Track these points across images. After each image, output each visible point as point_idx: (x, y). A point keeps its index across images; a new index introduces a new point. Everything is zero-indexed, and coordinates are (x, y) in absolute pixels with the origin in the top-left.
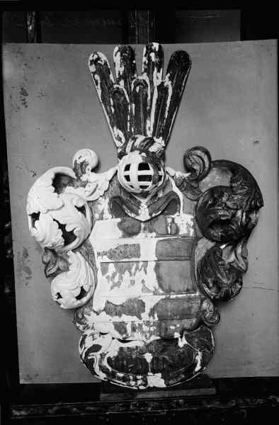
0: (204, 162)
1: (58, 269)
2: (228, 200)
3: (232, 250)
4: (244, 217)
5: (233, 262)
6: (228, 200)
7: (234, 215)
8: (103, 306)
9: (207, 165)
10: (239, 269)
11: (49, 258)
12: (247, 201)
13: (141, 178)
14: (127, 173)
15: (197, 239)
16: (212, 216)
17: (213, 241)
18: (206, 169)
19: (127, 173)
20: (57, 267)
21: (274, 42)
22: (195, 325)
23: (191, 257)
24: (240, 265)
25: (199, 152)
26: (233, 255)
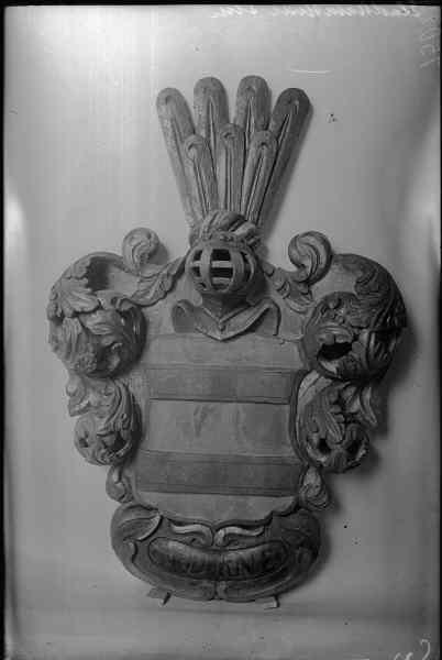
0: (317, 252)
1: (89, 405)
2: (348, 313)
3: (355, 394)
4: (372, 342)
5: (356, 413)
6: (348, 313)
7: (356, 338)
8: (353, 346)
9: (323, 259)
10: (365, 423)
11: (75, 388)
12: (379, 317)
13: (215, 272)
14: (197, 263)
15: (303, 374)
16: (324, 336)
17: (327, 377)
18: (322, 266)
19: (197, 263)
20: (86, 402)
21: (435, 9)
22: (290, 507)
23: (292, 400)
24: (367, 418)
25: (312, 240)
26: (358, 401)
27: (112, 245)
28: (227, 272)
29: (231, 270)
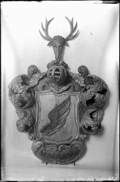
13: (55, 74)
14: (51, 72)
19: (51, 72)
27: (26, 73)
28: (59, 75)
29: (60, 74)
